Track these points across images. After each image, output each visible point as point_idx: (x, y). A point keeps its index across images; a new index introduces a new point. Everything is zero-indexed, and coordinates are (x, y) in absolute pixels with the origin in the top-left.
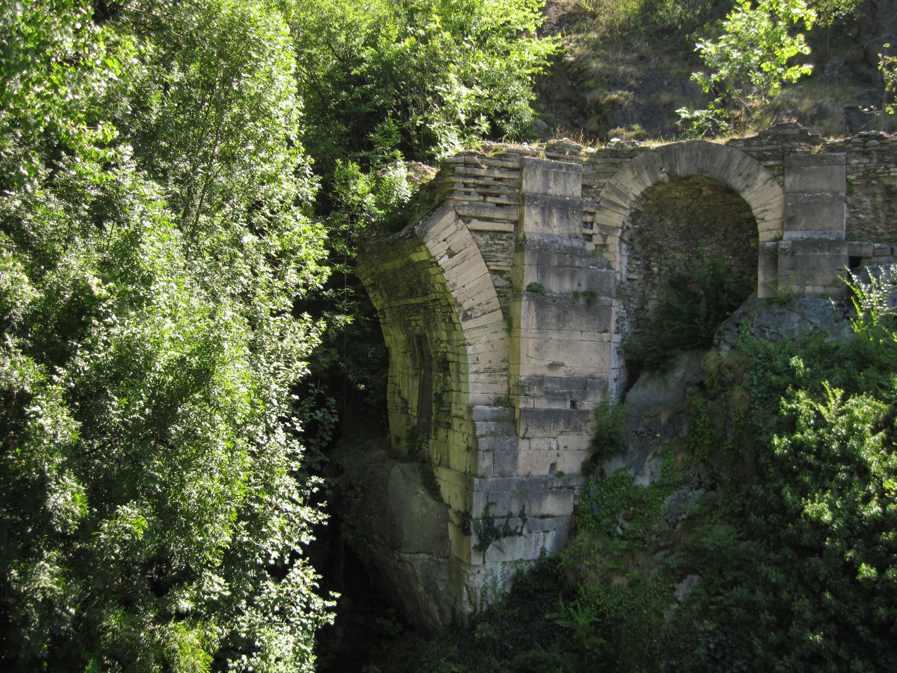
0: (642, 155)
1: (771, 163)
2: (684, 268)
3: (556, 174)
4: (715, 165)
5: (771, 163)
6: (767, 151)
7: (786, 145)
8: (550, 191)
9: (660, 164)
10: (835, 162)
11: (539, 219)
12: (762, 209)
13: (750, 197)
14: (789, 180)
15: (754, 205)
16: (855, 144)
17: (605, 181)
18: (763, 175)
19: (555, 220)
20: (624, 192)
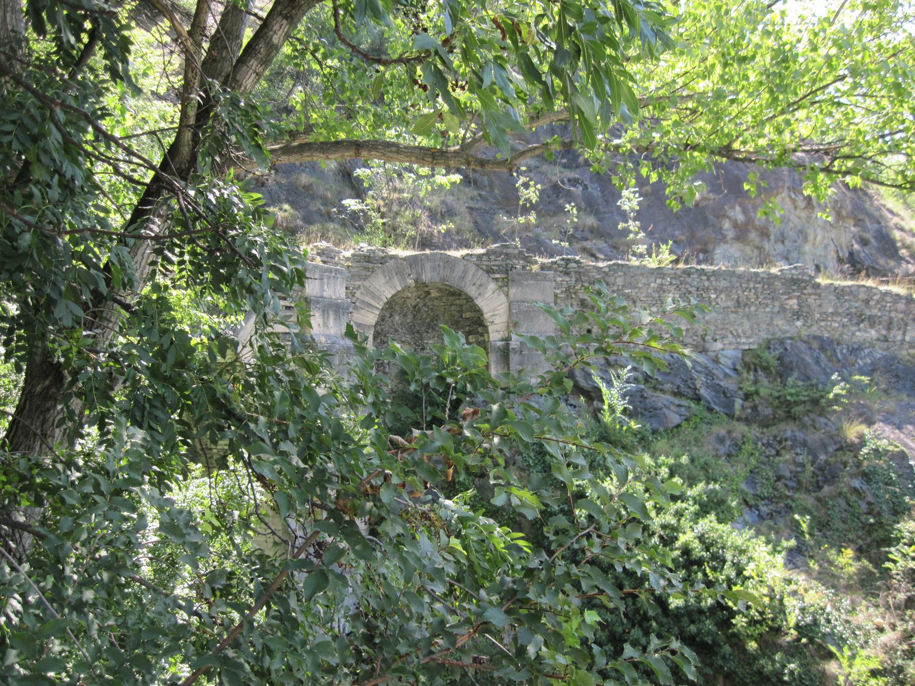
0: (392, 262)
1: (498, 276)
3: (329, 278)
5: (498, 276)
8: (325, 294)
9: (409, 271)
10: (545, 278)
14: (513, 291)
15: (485, 310)
16: (559, 266)
18: (492, 286)
19: (331, 321)
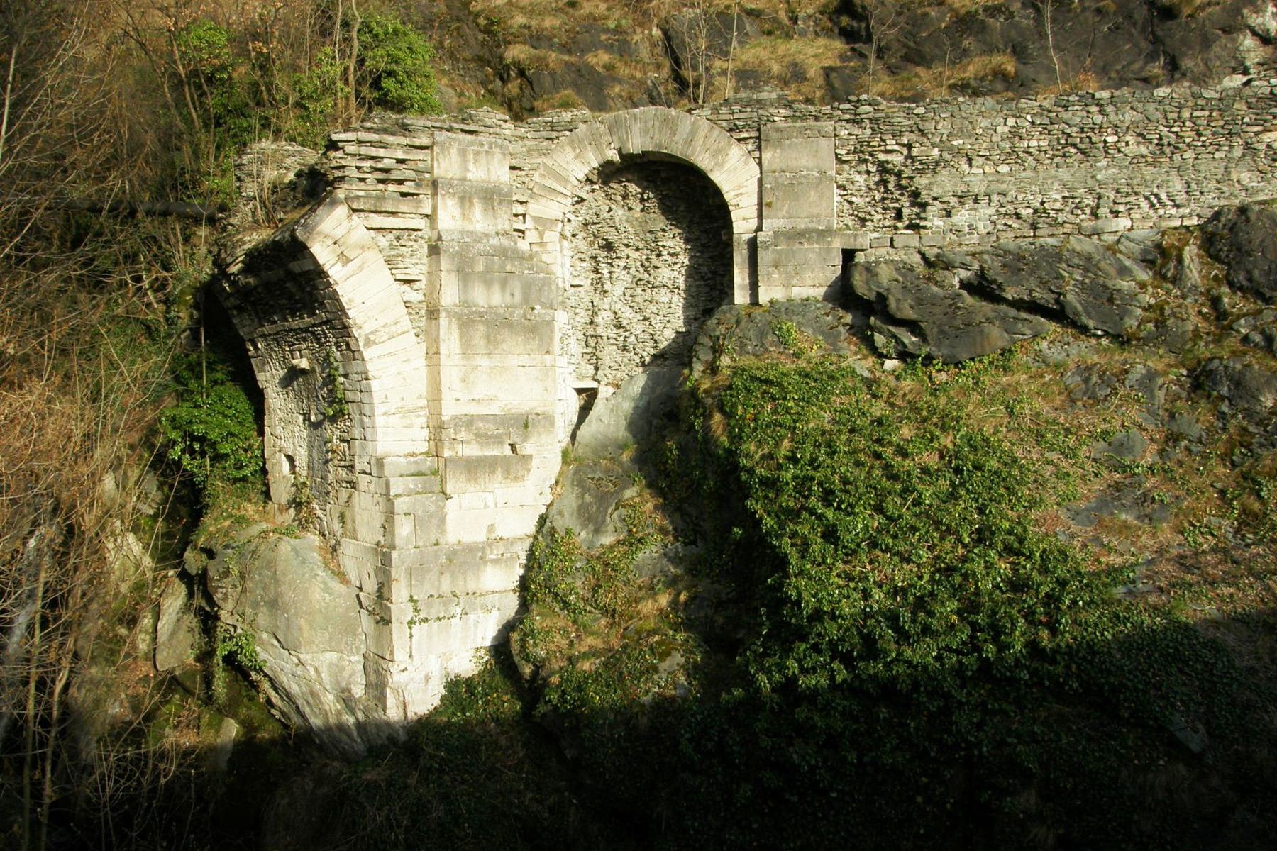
2: (642, 270)
3: (477, 153)
4: (676, 138)
5: (745, 135)
6: (738, 119)
7: (760, 112)
8: (469, 176)
11: (457, 212)
12: (737, 192)
13: (720, 179)
17: (539, 161)
20: (564, 174)
